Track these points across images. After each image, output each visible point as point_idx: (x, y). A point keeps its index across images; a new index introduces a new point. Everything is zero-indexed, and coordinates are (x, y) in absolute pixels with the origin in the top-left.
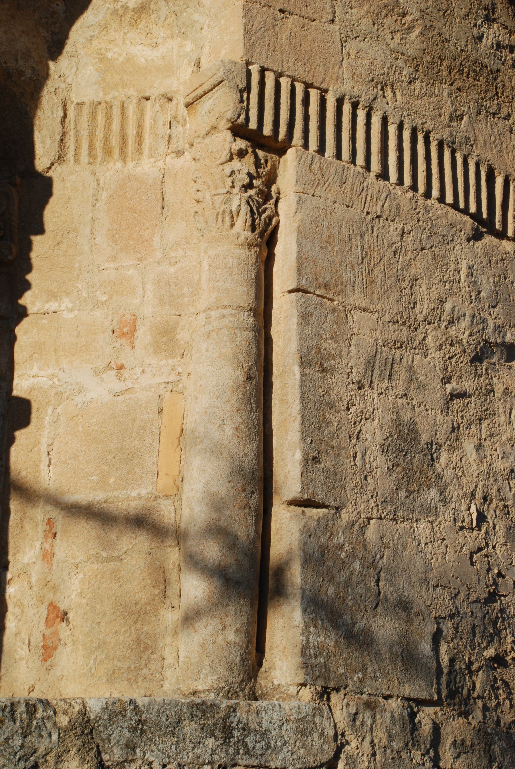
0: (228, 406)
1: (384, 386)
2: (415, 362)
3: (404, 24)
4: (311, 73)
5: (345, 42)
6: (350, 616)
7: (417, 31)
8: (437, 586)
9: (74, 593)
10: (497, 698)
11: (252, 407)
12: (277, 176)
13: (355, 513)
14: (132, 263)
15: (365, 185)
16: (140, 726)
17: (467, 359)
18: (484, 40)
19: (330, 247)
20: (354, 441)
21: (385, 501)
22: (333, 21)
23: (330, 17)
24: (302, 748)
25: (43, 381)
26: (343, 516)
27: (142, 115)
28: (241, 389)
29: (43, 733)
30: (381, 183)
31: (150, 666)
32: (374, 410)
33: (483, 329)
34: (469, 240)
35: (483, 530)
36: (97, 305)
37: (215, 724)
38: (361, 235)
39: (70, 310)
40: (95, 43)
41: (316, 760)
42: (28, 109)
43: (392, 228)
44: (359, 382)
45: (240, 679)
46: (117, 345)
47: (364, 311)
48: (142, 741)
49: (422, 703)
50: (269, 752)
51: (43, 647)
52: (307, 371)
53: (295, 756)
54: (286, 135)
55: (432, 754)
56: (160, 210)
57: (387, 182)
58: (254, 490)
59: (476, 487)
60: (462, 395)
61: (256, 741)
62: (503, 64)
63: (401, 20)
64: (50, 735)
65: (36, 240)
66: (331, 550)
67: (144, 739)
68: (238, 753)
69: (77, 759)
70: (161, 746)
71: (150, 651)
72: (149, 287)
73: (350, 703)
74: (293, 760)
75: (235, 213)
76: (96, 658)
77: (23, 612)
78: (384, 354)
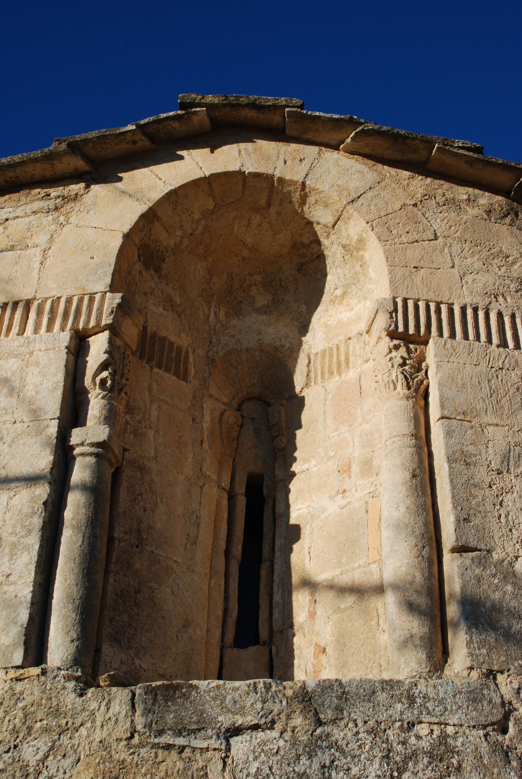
3: (508, 261)
4: (440, 296)
5: (463, 276)
6: (506, 622)
9: (328, 635)
11: (418, 494)
12: (426, 357)
13: (504, 554)
14: (346, 429)
15: (488, 351)
16: (345, 696)
19: (464, 390)
20: (498, 507)
23: (451, 265)
24: (474, 711)
25: (305, 511)
26: (494, 556)
27: (348, 347)
28: (409, 483)
29: (276, 701)
30: (502, 349)
31: (373, 672)
32: (512, 486)
36: (329, 459)
37: (401, 694)
38: (488, 381)
39: (315, 466)
40: (322, 320)
41: (487, 720)
42: (287, 363)
43: (513, 375)
44: (498, 470)
45: (427, 670)
46: (341, 478)
47: (497, 425)
48: (347, 706)
50: (447, 713)
51: (313, 672)
52: (454, 465)
53: (469, 717)
54: (425, 332)
56: (359, 394)
57: (507, 349)
58: (425, 545)
61: (435, 706)
63: (506, 260)
64: (281, 702)
66: (485, 578)
67: (349, 704)
68: (422, 714)
69: (301, 717)
70: (361, 709)
71: (372, 662)
73: (513, 681)
74: (468, 719)
75: (395, 381)
76: (343, 673)
77: (301, 652)
78: (517, 451)
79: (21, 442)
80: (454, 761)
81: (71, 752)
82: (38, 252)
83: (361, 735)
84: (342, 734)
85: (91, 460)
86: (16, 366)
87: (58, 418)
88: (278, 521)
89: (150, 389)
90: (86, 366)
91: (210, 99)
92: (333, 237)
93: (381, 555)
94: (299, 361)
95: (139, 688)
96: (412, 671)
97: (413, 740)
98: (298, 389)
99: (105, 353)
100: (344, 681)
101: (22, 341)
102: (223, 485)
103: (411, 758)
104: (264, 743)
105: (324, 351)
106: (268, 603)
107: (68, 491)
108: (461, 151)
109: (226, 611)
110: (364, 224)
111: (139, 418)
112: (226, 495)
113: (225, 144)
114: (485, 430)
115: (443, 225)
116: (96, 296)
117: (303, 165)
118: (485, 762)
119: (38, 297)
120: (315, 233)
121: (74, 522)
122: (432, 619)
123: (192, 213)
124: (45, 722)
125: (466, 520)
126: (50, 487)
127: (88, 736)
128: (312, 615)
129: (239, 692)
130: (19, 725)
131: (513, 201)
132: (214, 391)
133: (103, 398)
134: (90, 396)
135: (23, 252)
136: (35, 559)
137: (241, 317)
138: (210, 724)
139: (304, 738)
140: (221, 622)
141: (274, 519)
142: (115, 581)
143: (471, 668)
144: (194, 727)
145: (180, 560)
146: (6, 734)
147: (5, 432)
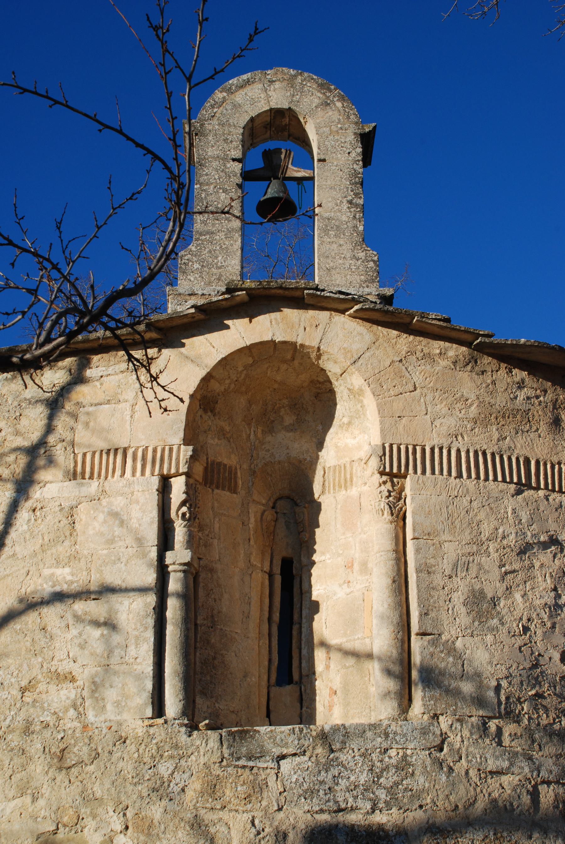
0: (385, 595)
1: (464, 575)
2: (482, 560)
7: (475, 405)
8: (498, 664)
10: (537, 713)
17: (514, 554)
18: (518, 398)
20: (447, 603)
21: (466, 628)
22: (426, 414)
23: (425, 413)
25: (322, 591)
27: (352, 468)
33: (524, 537)
34: (513, 496)
35: (528, 635)
36: (339, 555)
37: (381, 732)
39: (329, 559)
40: (333, 440)
43: (464, 500)
46: (347, 572)
49: (490, 718)
52: (420, 575)
55: (496, 740)
56: (359, 510)
57: (462, 479)
59: (523, 615)
60: (514, 571)
62: (533, 405)
64: (309, 739)
65: (317, 530)
72: (357, 545)
79: (133, 562)
80: (410, 770)
81: (188, 770)
82: (127, 406)
83: (356, 758)
84: (345, 757)
85: (181, 575)
86: (123, 503)
87: (157, 546)
88: (304, 596)
89: (213, 508)
90: (171, 502)
91: (248, 284)
92: (340, 381)
93: (372, 633)
94: (317, 472)
95: (224, 732)
96: (388, 714)
97: (387, 759)
98: (316, 496)
99: (183, 493)
100: (346, 725)
101: (125, 482)
102: (265, 569)
103: (385, 770)
104: (300, 764)
105: (335, 467)
106: (298, 655)
107: (167, 597)
108: (433, 322)
109: (270, 661)
110: (363, 381)
111: (207, 532)
112: (267, 577)
113: (260, 314)
114: (442, 546)
115: (421, 377)
116: (174, 447)
117: (318, 331)
118: (428, 769)
119: (132, 446)
120: (328, 377)
121: (174, 621)
122: (402, 680)
123: (237, 368)
124: (170, 752)
125: (426, 614)
126: (156, 597)
127: (196, 761)
128: (328, 667)
129: (284, 734)
130: (155, 754)
131: (474, 350)
132: (255, 497)
133: (184, 527)
134: (175, 525)
135: (117, 405)
136: (152, 647)
137: (274, 434)
138: (268, 753)
139: (323, 760)
140: (267, 669)
141: (301, 594)
142: (200, 654)
143: (424, 713)
144: (258, 755)
145: (239, 631)
146: (148, 758)
147: (121, 554)
